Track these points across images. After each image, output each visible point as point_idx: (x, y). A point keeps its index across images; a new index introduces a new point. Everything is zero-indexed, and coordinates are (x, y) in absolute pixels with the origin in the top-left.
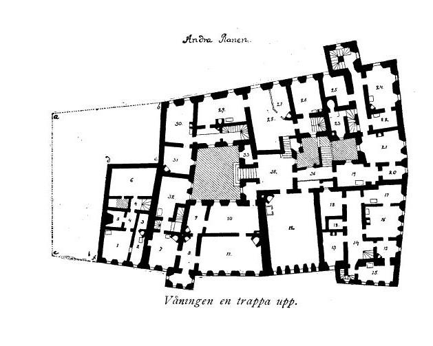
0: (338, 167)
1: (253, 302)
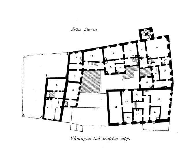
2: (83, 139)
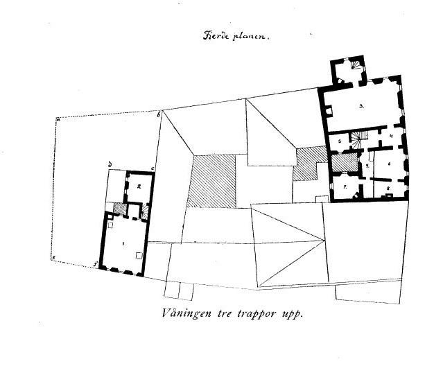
1: (253, 315)
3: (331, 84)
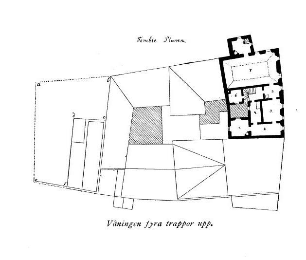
0: (241, 101)
1: (177, 224)
2: (129, 225)
3: (228, 55)
